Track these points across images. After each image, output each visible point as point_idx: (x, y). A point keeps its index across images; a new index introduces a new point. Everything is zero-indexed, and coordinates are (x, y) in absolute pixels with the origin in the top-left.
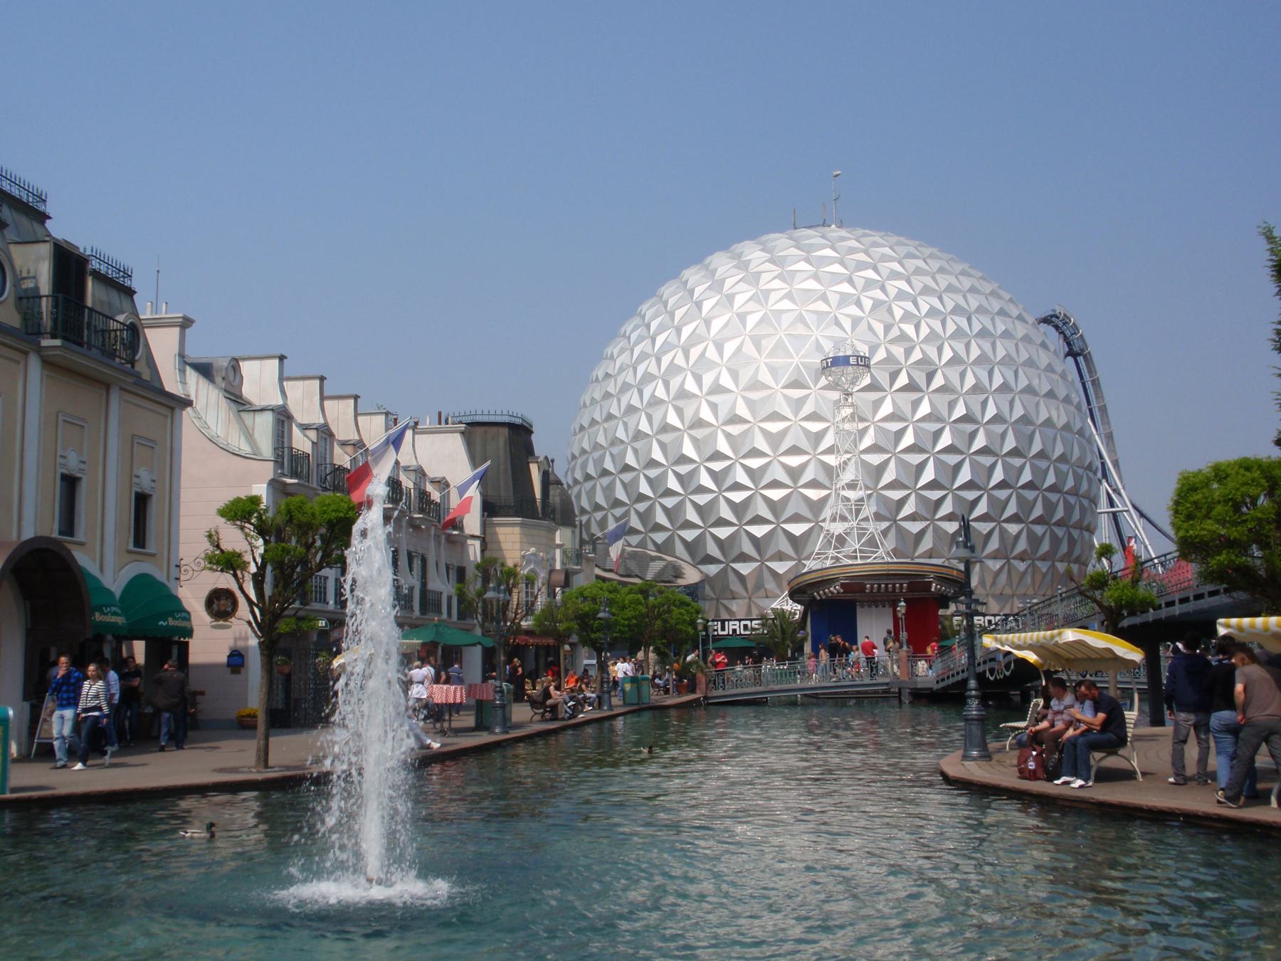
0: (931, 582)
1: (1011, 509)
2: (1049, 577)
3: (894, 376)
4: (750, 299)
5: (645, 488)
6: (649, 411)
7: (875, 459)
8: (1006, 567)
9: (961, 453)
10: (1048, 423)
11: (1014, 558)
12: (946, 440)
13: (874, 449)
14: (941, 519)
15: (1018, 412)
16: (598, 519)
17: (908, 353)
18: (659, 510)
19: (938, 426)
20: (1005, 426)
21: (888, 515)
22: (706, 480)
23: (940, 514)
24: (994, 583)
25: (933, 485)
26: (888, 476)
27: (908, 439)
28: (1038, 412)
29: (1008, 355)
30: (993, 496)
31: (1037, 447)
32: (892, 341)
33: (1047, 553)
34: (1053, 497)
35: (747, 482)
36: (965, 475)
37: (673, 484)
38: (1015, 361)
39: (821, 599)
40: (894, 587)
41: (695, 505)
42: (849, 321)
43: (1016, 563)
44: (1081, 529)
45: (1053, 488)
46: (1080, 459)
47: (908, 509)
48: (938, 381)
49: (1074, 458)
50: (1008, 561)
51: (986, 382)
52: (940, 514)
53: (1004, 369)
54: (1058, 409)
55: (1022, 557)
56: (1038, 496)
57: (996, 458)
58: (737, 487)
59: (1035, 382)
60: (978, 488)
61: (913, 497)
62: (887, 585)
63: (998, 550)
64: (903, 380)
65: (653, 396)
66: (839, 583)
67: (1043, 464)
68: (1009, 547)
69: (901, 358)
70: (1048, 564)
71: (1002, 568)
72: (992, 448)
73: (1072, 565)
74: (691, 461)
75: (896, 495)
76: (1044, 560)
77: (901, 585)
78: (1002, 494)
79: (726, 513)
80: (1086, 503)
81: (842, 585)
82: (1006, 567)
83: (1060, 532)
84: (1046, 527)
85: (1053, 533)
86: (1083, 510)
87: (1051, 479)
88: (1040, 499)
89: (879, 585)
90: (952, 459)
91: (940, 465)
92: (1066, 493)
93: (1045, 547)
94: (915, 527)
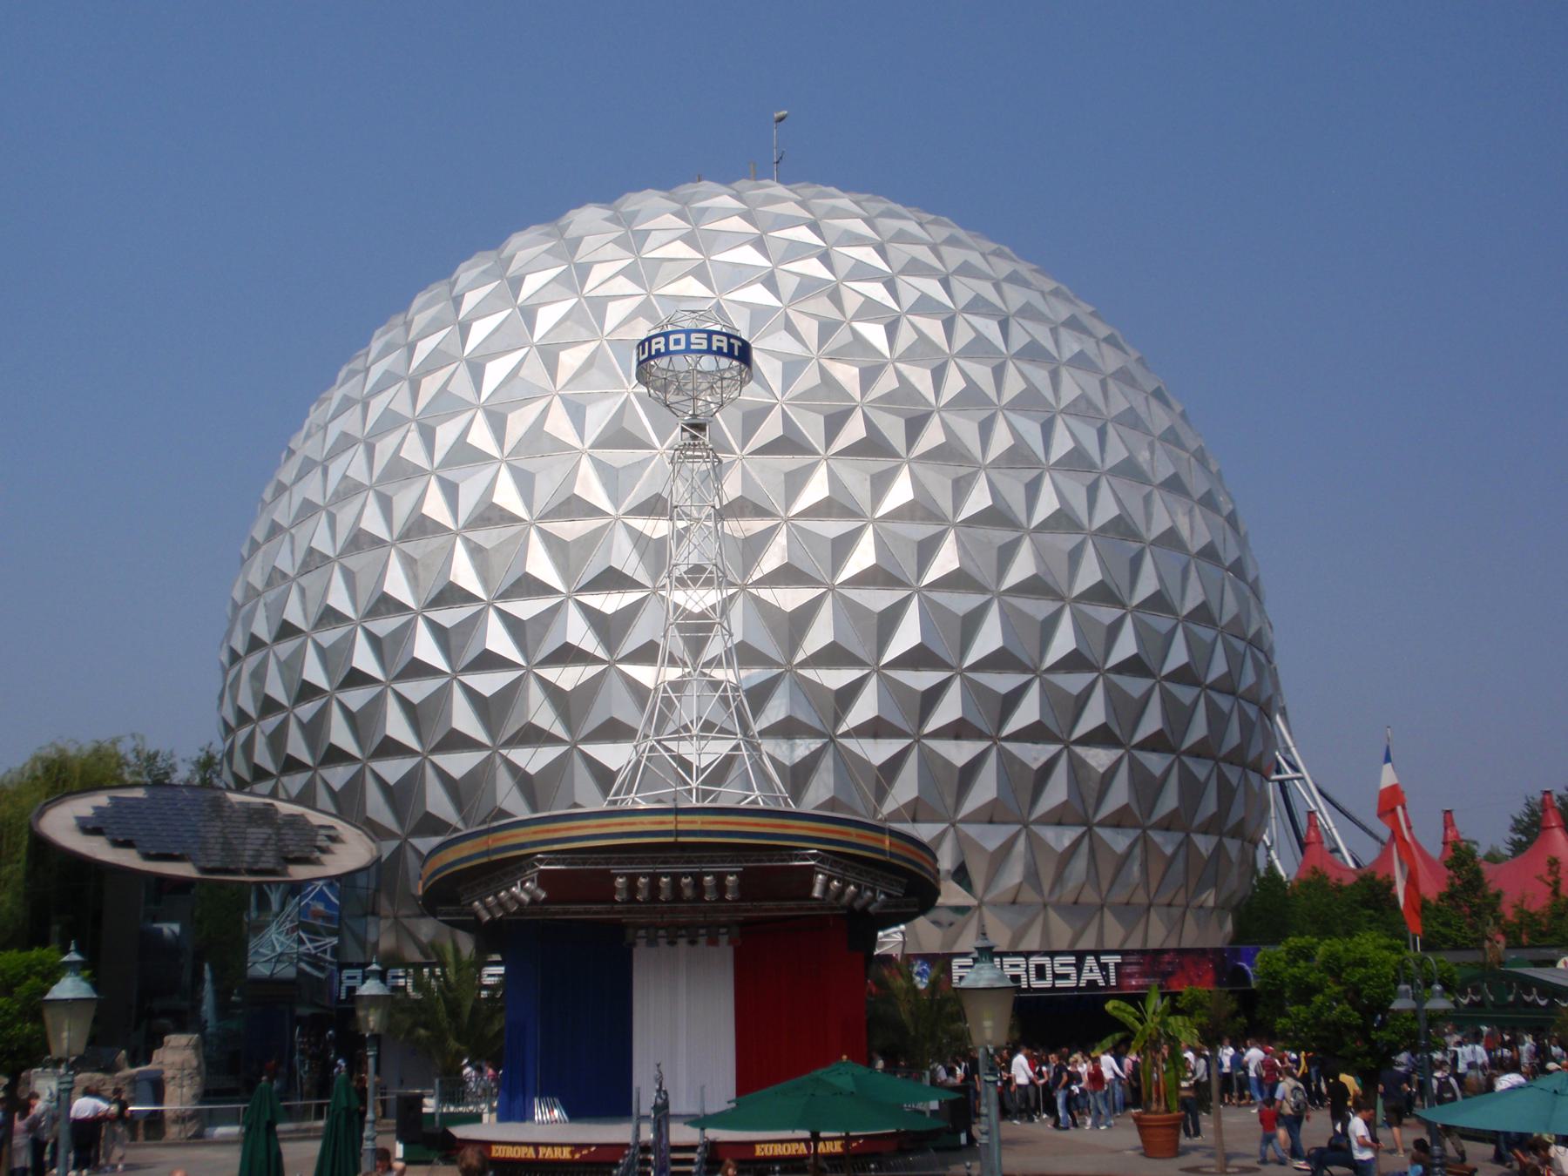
0: (811, 871)
1: (1094, 715)
2: (1179, 865)
3: (835, 424)
4: (622, 272)
5: (364, 659)
6: (386, 489)
7: (789, 599)
8: (1084, 847)
9: (981, 589)
10: (1171, 539)
11: (1102, 824)
12: (946, 560)
13: (787, 575)
14: (938, 734)
15: (1107, 510)
16: (306, 718)
17: (868, 377)
18: (459, 701)
19: (929, 530)
20: (1078, 538)
21: (817, 725)
22: (498, 640)
23: (935, 722)
24: (1059, 878)
25: (917, 658)
26: (820, 635)
27: (863, 557)
28: (1148, 516)
29: (1084, 397)
30: (1051, 684)
31: (1147, 586)
32: (836, 356)
33: (1175, 812)
34: (1185, 694)
35: (590, 644)
36: (989, 639)
37: (426, 649)
38: (1098, 410)
39: (492, 921)
40: (654, 887)
41: (471, 694)
42: (815, 325)
43: (1105, 834)
44: (1244, 765)
45: (1183, 675)
46: (1236, 619)
47: (864, 709)
48: (933, 436)
49: (1226, 618)
50: (1090, 829)
51: (1036, 444)
52: (935, 722)
53: (1075, 424)
54: (1190, 512)
55: (1119, 820)
56: (1199, 696)
57: (1057, 605)
58: (568, 655)
59: (1143, 456)
60: (1020, 667)
61: (872, 684)
62: (676, 878)
63: (993, 803)
64: (854, 431)
65: (396, 458)
66: (532, 873)
67: (1162, 623)
68: (1091, 801)
69: (854, 387)
70: (1178, 836)
71: (1076, 844)
72: (1049, 580)
73: (1227, 842)
74: (470, 598)
75: (835, 679)
76: (1168, 829)
77: (720, 877)
78: (1074, 683)
79: (544, 716)
80: (1252, 712)
81: (545, 879)
82: (1086, 842)
83: (1201, 770)
84: (1172, 757)
85: (1184, 770)
86: (1247, 726)
87: (1178, 656)
88: (1156, 698)
89: (654, 878)
90: (962, 603)
91: (931, 615)
92: (1212, 687)
93: (1169, 801)
94: (878, 752)
